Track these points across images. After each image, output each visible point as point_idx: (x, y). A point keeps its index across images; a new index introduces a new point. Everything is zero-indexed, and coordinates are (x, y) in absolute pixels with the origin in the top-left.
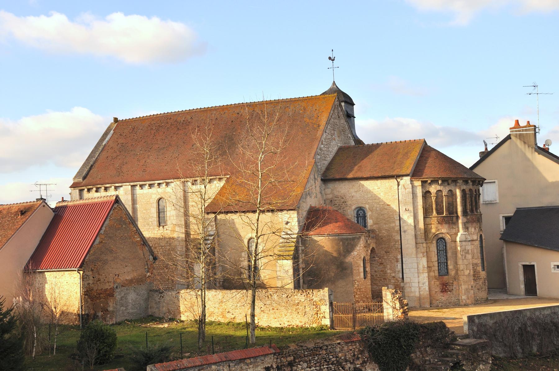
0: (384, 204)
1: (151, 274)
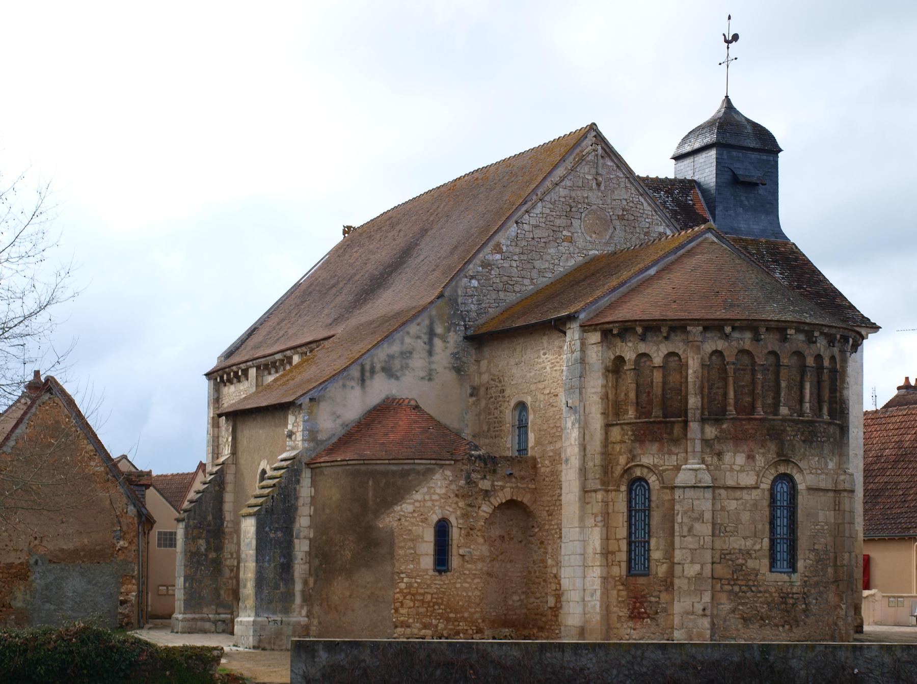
1: (130, 543)
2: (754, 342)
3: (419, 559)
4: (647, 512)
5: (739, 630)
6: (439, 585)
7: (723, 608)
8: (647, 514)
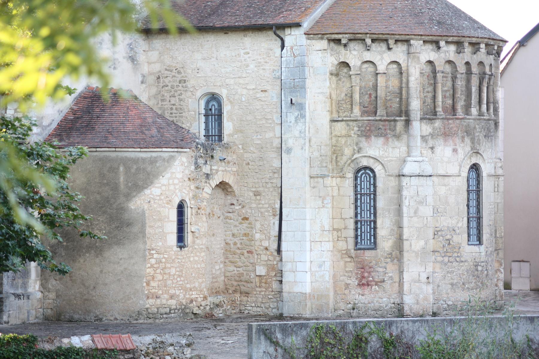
2: (457, 54)
3: (166, 237)
4: (372, 196)
5: (449, 294)
6: (180, 259)
7: (437, 276)
8: (372, 197)
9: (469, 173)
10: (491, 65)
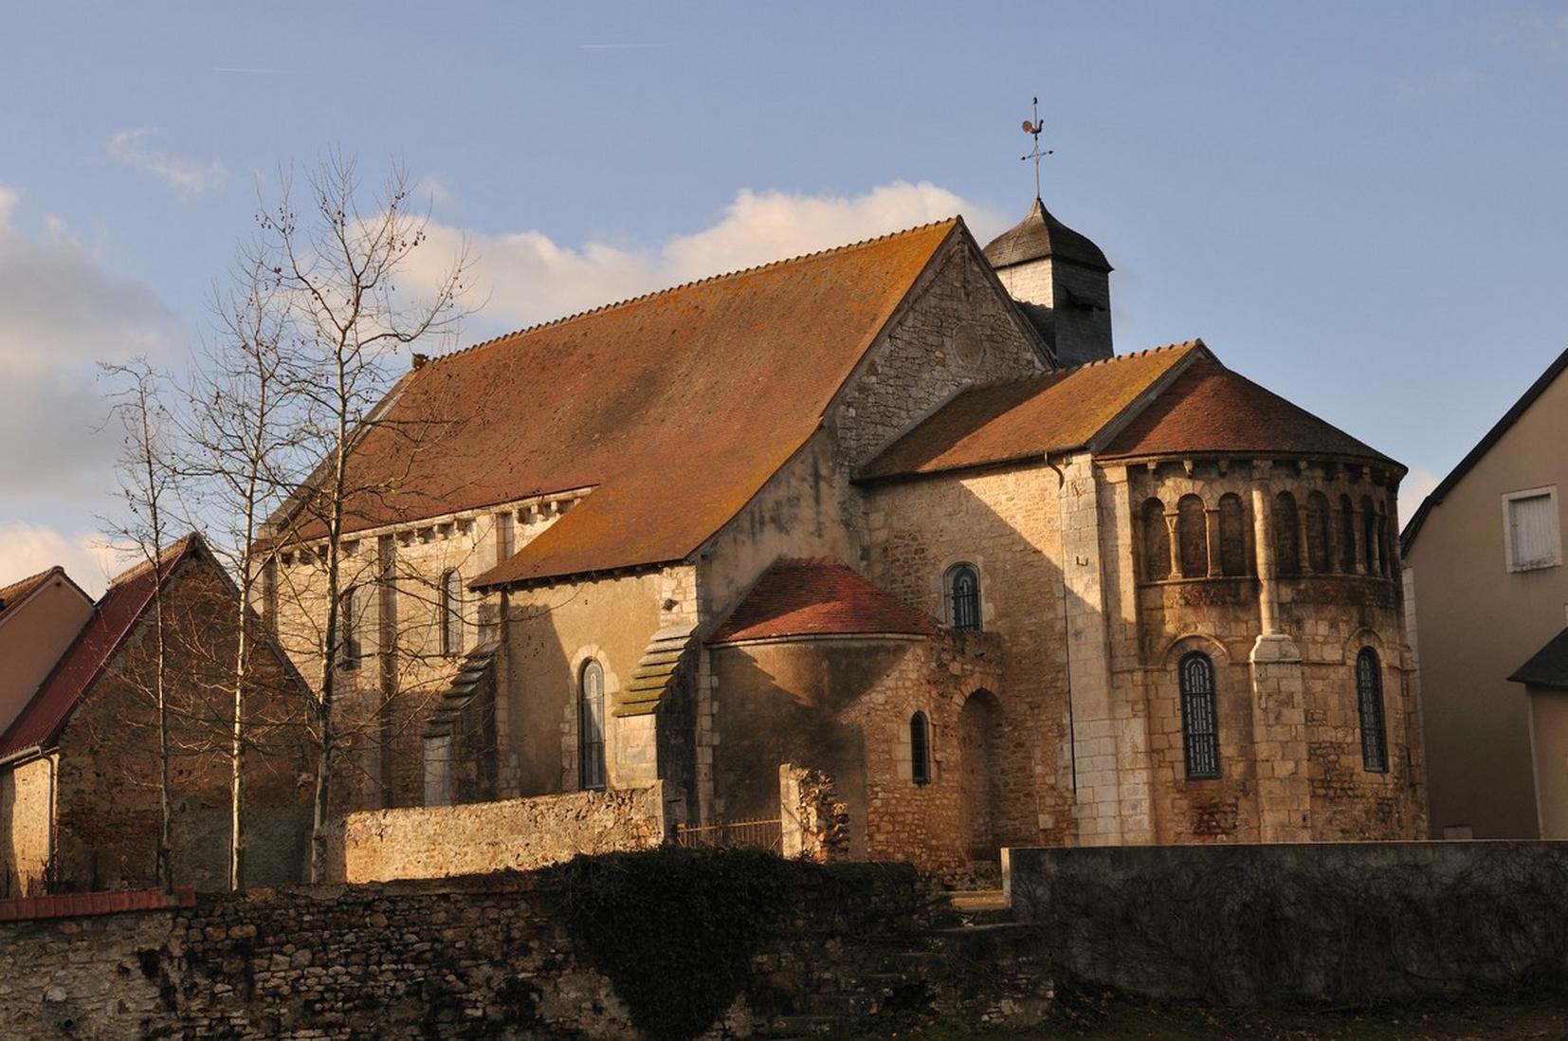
0: (1025, 549)
3: (896, 766)
9: (1358, 661)
10: (1382, 503)
